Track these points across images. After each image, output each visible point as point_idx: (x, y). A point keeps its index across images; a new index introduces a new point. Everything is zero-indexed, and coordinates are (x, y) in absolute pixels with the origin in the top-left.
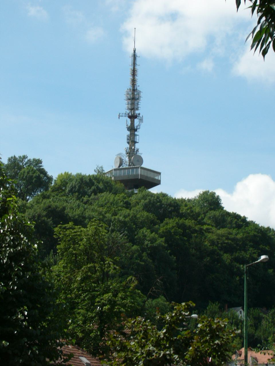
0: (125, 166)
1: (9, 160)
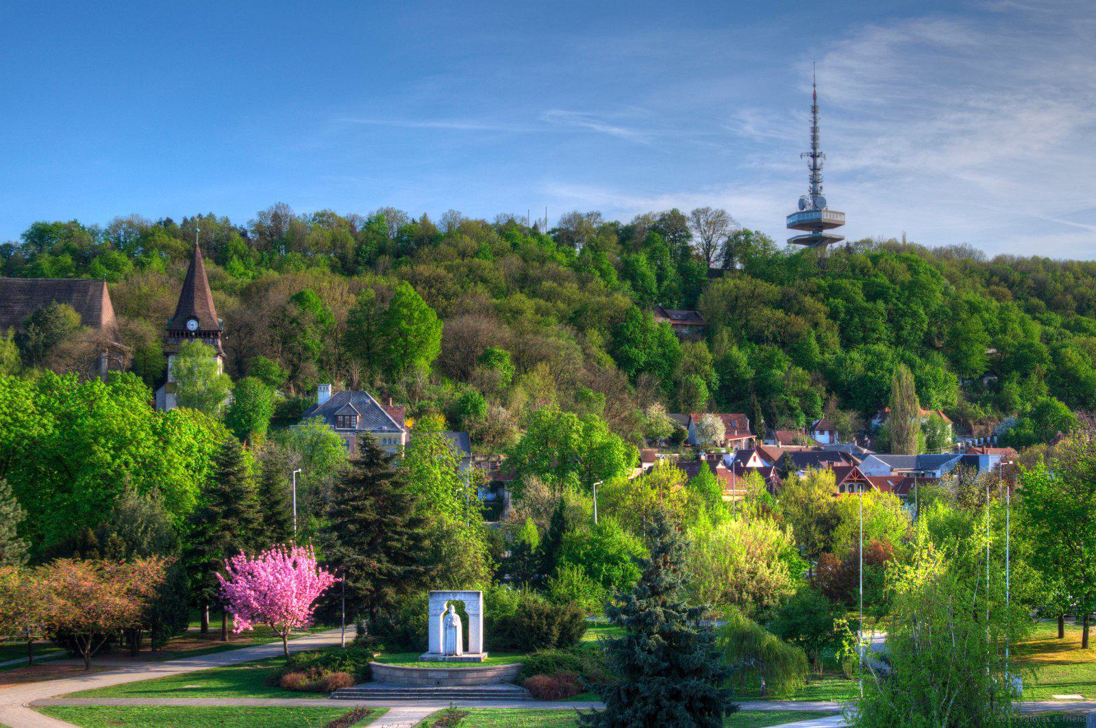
0: (808, 208)
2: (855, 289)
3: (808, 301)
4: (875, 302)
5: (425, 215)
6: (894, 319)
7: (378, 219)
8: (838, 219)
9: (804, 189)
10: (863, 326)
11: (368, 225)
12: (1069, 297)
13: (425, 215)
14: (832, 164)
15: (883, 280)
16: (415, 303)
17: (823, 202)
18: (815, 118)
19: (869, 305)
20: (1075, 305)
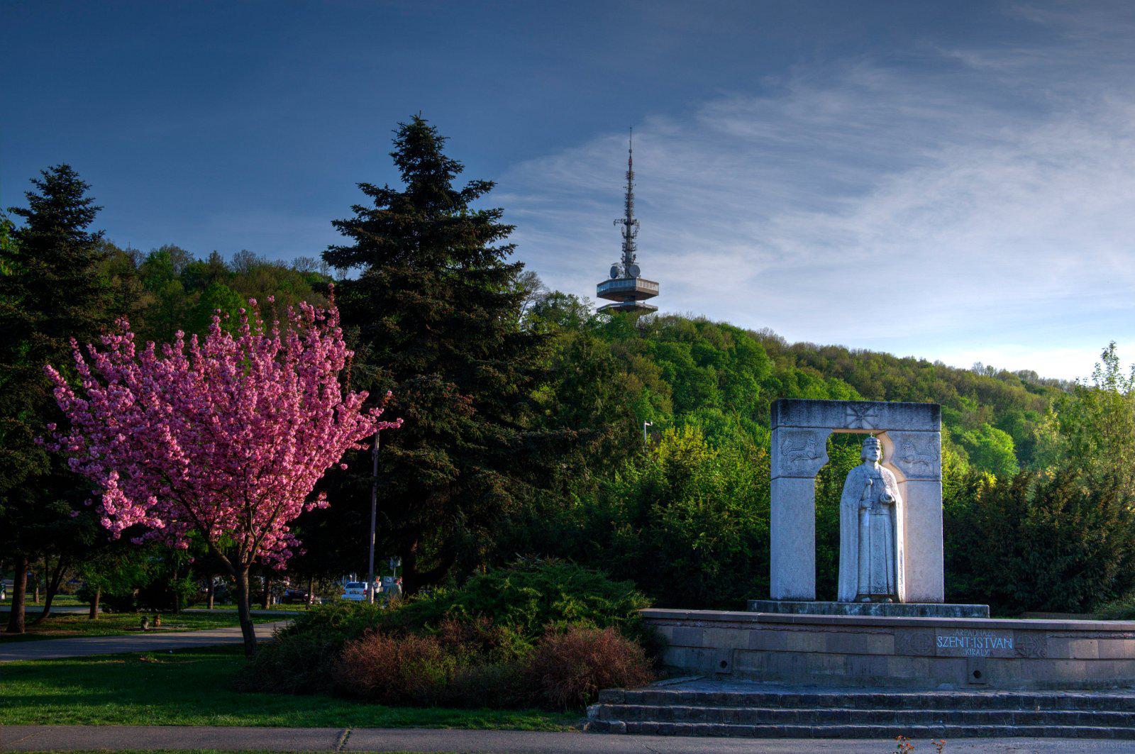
0: (622, 276)
1: (237, 257)
2: (684, 352)
3: (640, 360)
4: (705, 367)
5: (215, 254)
6: (726, 385)
7: (162, 255)
8: (654, 288)
9: (617, 258)
10: (695, 390)
11: (151, 261)
12: (878, 384)
13: (215, 254)
14: (642, 236)
15: (708, 346)
16: (232, 299)
17: (637, 270)
18: (630, 184)
19: (701, 370)
20: (884, 392)
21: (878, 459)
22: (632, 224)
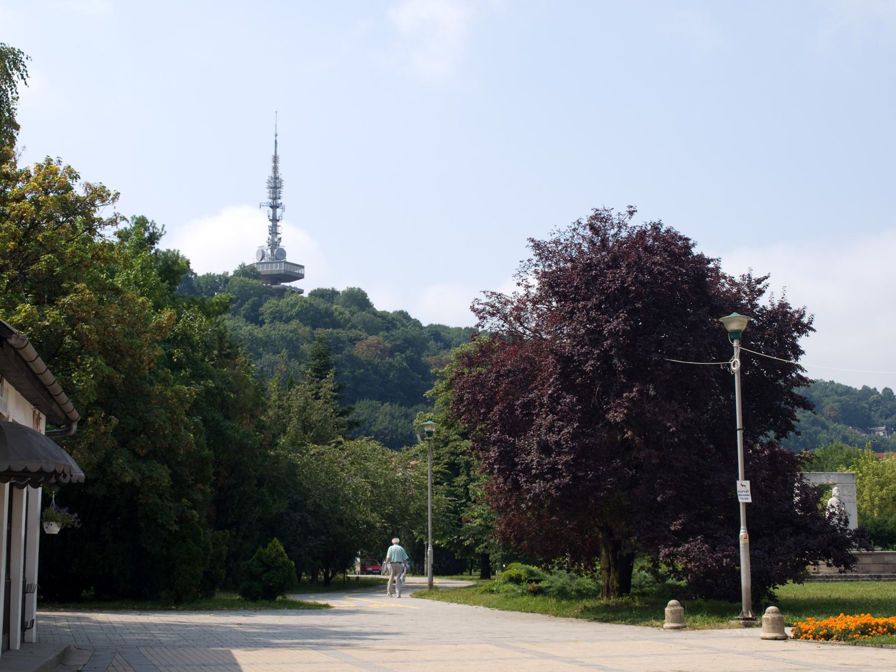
21: (154, 381)
22: (278, 207)
